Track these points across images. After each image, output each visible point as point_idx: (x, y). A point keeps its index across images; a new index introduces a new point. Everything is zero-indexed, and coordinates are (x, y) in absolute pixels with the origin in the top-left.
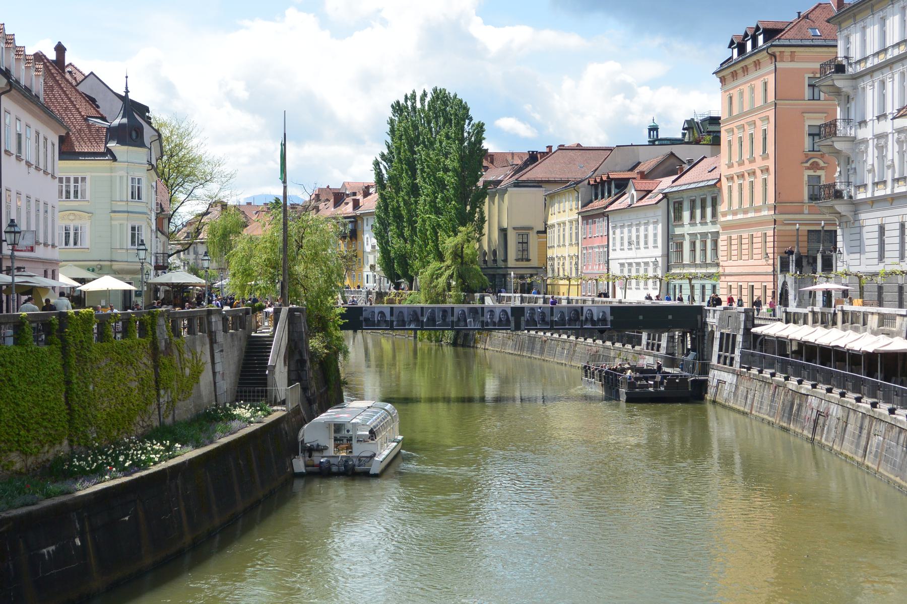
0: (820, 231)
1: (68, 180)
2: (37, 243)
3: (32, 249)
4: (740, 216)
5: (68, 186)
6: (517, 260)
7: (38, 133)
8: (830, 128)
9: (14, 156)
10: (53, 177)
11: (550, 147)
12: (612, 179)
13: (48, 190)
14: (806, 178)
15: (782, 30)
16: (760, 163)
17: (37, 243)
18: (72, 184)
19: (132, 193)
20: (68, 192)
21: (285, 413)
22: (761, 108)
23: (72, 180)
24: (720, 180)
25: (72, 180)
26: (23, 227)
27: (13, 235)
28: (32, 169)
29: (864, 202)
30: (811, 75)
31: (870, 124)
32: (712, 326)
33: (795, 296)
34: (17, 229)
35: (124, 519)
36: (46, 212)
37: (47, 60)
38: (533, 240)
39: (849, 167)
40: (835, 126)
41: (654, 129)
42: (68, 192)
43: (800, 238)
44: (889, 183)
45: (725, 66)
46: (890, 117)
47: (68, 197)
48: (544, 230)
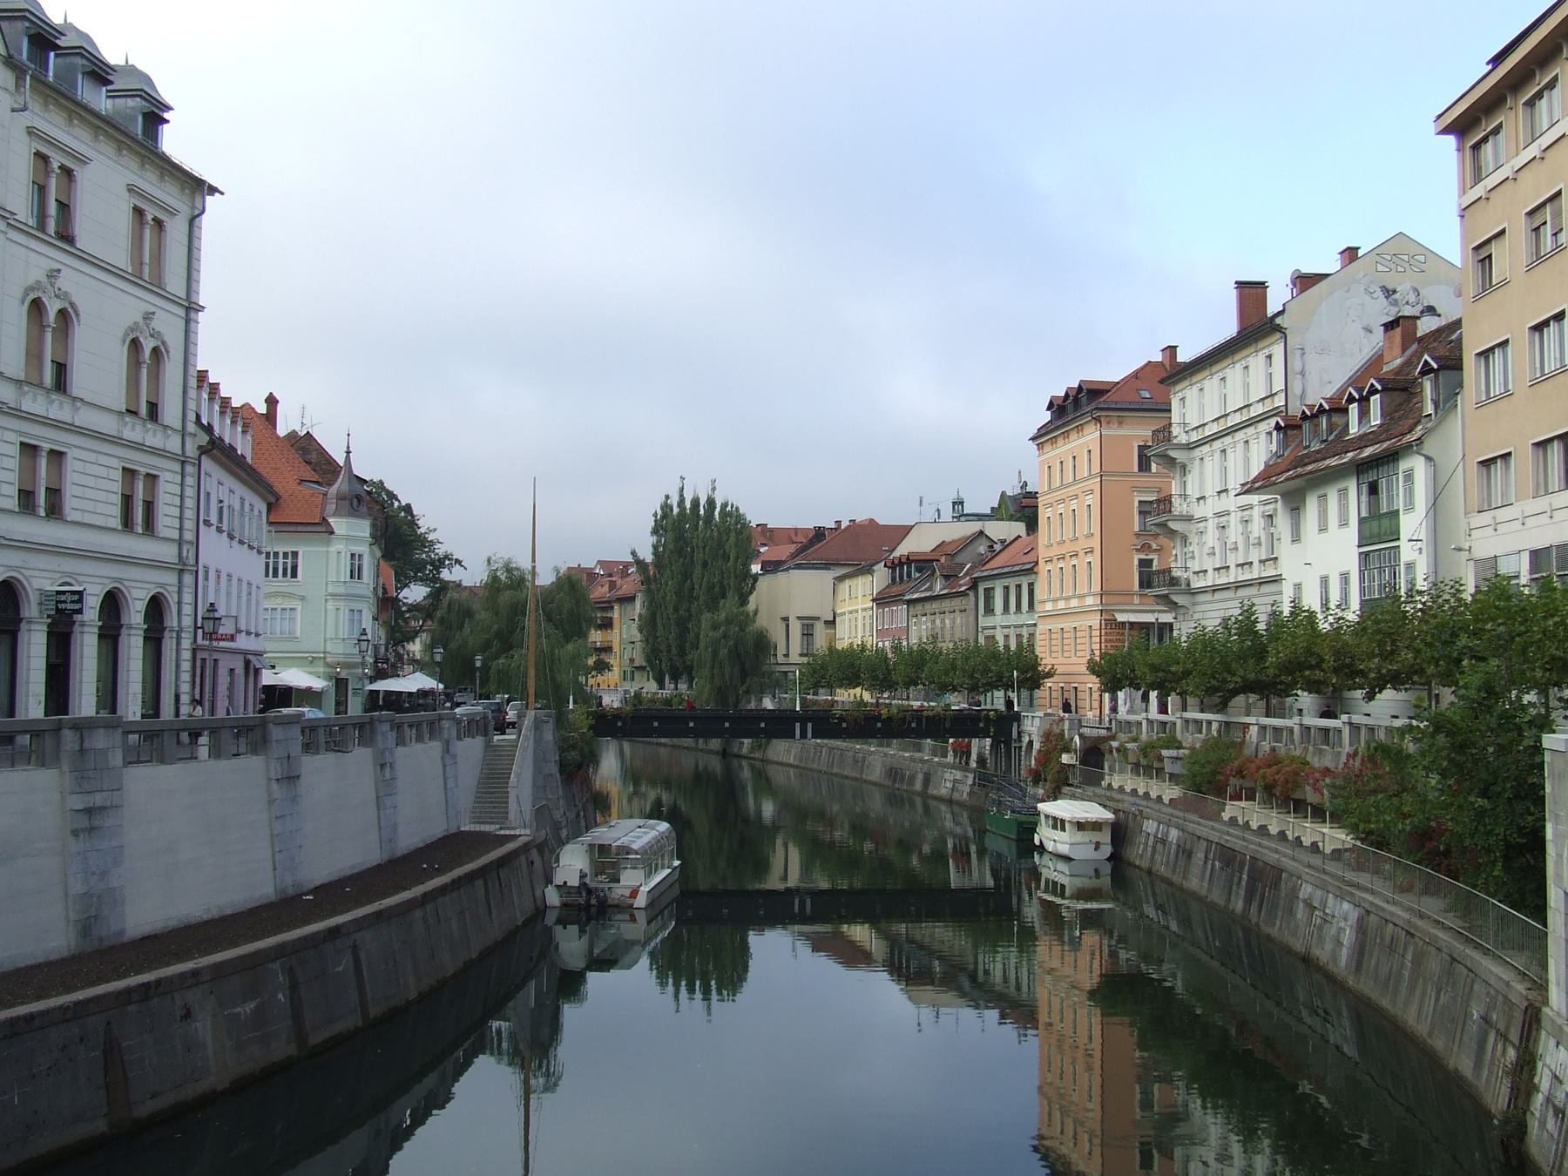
0: (1153, 623)
1: (276, 554)
2: (239, 631)
3: (232, 638)
4: (1074, 603)
5: (276, 563)
6: (801, 655)
7: (242, 500)
8: (1165, 502)
9: (214, 527)
10: (259, 552)
11: (838, 522)
12: (913, 561)
13: (250, 566)
14: (1136, 563)
15: (1108, 391)
16: (1083, 544)
17: (239, 631)
18: (281, 560)
19: (351, 571)
20: (110, 634)
21: (530, 838)
22: (1084, 480)
23: (281, 555)
24: (1037, 563)
25: (281, 555)
26: (221, 612)
27: (212, 622)
28: (235, 543)
29: (1203, 591)
30: (1142, 444)
31: (1209, 501)
32: (1030, 735)
33: (1126, 700)
34: (217, 615)
35: (337, 969)
36: (250, 594)
37: (256, 413)
38: (819, 629)
39: (1185, 550)
40: (1170, 502)
41: (958, 503)
42: (110, 634)
43: (1053, 636)
44: (1256, 564)
45: (1043, 431)
46: (1233, 493)
47: (275, 574)
48: (832, 619)
